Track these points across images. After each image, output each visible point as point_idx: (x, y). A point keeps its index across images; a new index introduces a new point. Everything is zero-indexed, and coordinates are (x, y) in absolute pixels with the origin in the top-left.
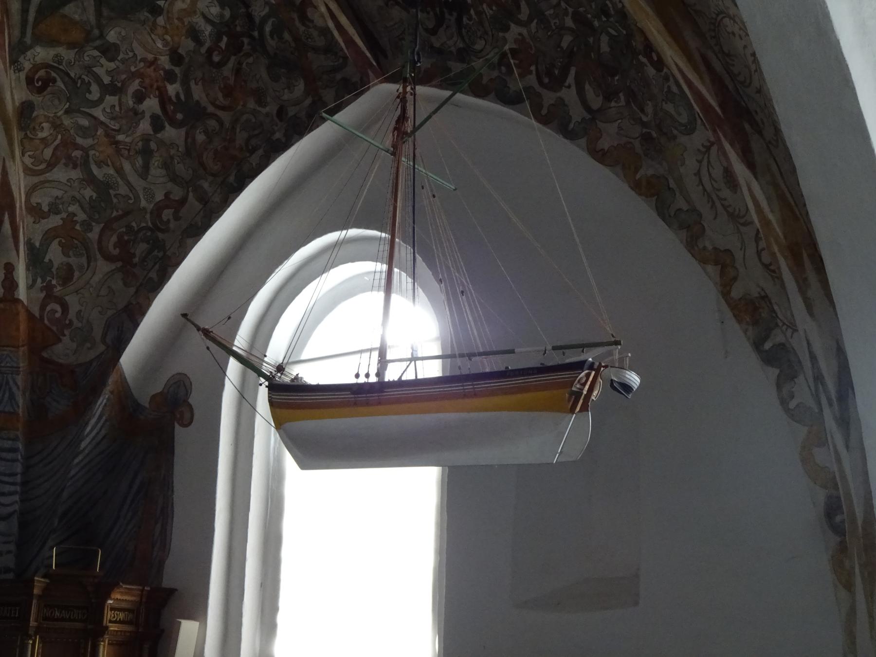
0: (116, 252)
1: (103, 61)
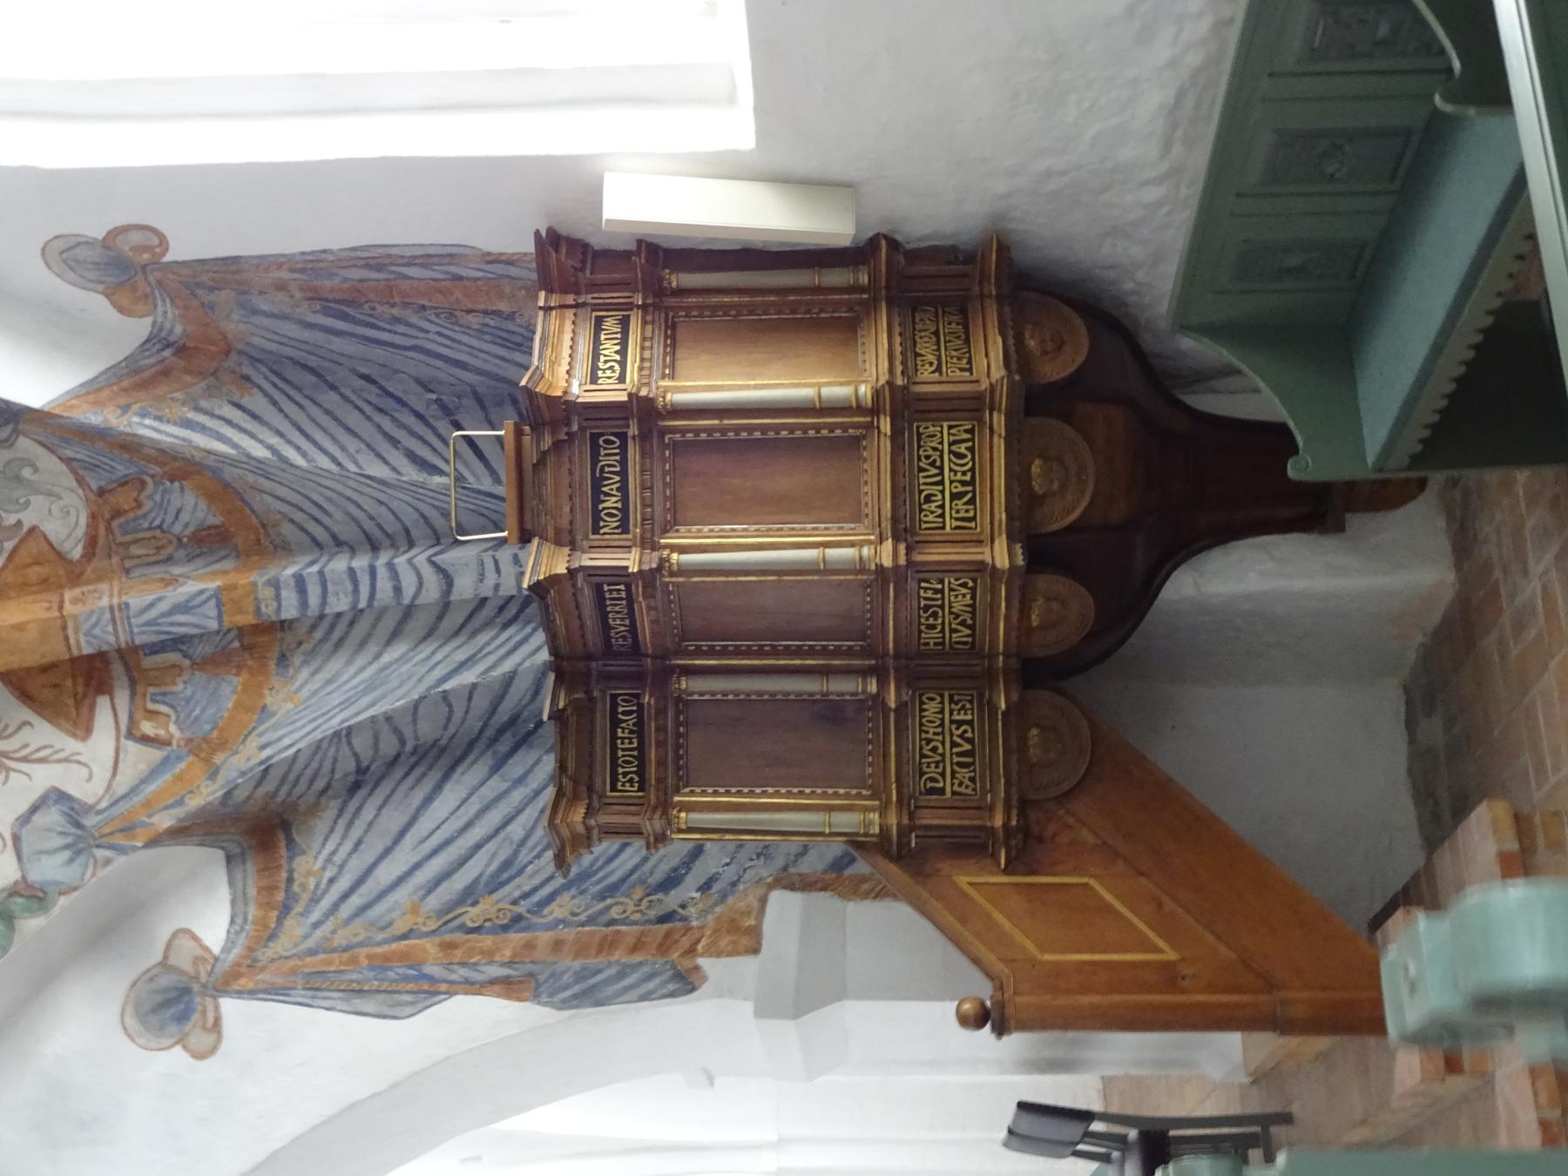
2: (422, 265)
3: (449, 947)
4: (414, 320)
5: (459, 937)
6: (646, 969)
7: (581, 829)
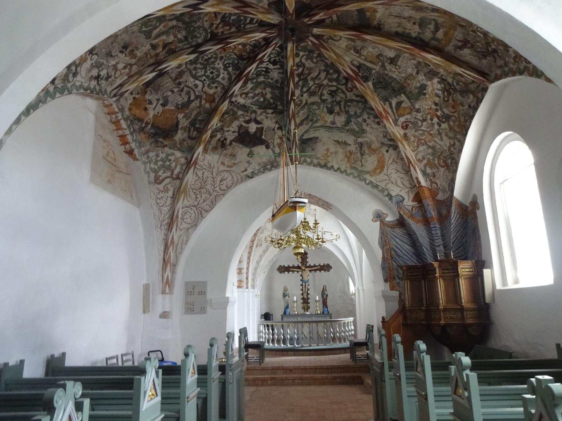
0: (444, 164)
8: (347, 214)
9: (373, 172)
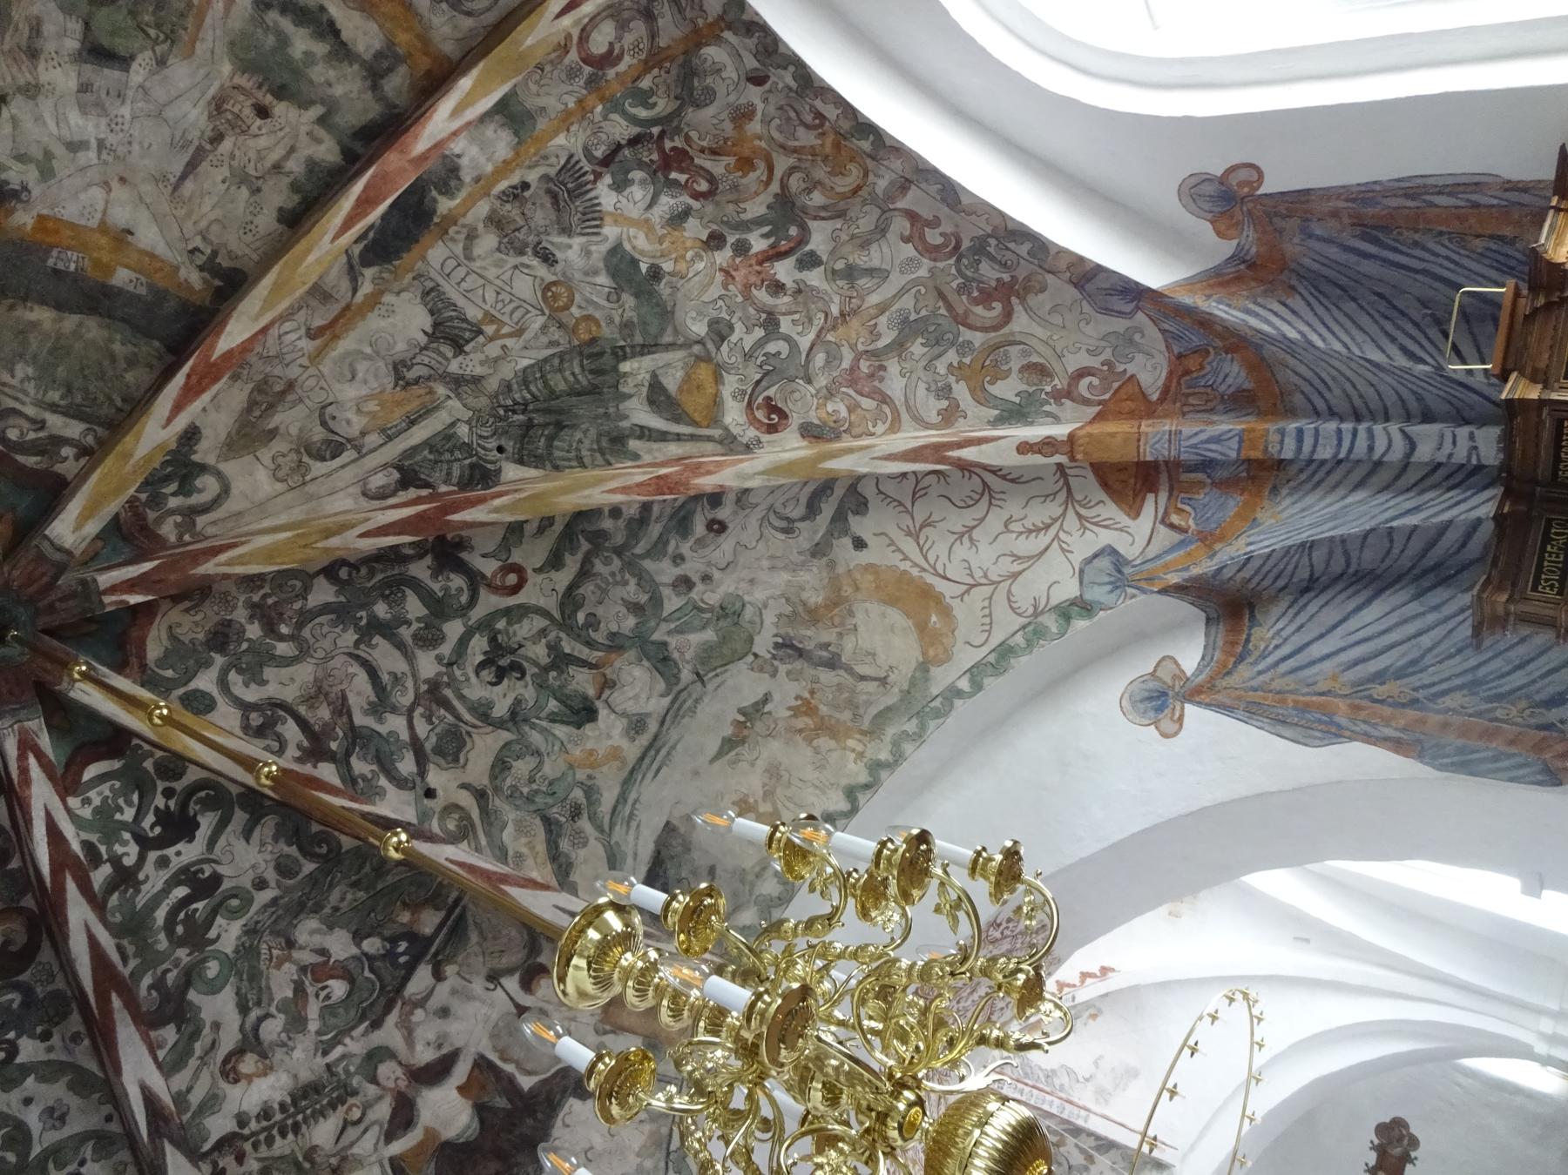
0: (998, 306)
1: (734, 338)
2: (1450, 194)
3: (1357, 708)
4: (1431, 245)
5: (1365, 703)
6: (1520, 760)
7: (1500, 610)
8: (1090, 847)
9: (934, 647)
